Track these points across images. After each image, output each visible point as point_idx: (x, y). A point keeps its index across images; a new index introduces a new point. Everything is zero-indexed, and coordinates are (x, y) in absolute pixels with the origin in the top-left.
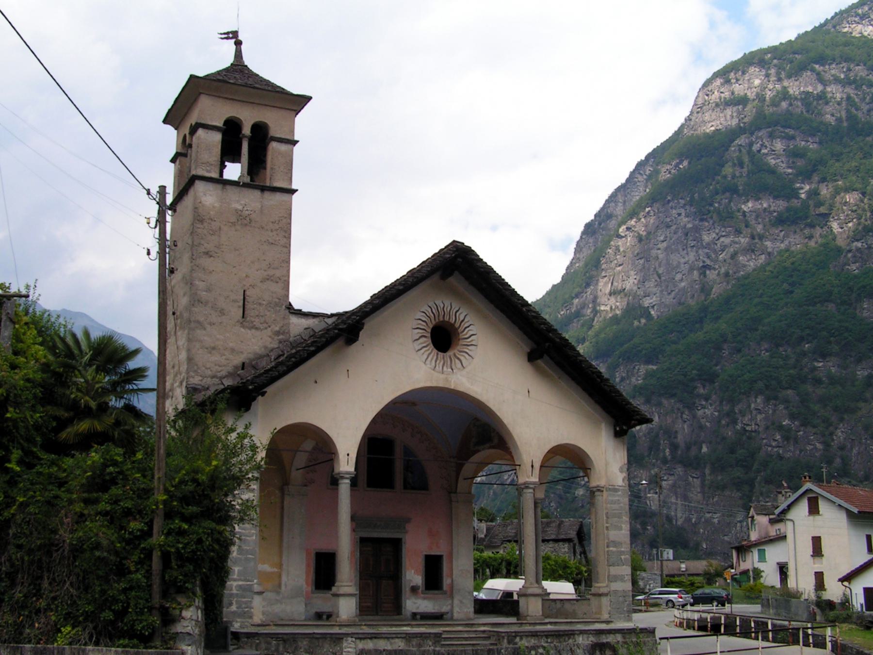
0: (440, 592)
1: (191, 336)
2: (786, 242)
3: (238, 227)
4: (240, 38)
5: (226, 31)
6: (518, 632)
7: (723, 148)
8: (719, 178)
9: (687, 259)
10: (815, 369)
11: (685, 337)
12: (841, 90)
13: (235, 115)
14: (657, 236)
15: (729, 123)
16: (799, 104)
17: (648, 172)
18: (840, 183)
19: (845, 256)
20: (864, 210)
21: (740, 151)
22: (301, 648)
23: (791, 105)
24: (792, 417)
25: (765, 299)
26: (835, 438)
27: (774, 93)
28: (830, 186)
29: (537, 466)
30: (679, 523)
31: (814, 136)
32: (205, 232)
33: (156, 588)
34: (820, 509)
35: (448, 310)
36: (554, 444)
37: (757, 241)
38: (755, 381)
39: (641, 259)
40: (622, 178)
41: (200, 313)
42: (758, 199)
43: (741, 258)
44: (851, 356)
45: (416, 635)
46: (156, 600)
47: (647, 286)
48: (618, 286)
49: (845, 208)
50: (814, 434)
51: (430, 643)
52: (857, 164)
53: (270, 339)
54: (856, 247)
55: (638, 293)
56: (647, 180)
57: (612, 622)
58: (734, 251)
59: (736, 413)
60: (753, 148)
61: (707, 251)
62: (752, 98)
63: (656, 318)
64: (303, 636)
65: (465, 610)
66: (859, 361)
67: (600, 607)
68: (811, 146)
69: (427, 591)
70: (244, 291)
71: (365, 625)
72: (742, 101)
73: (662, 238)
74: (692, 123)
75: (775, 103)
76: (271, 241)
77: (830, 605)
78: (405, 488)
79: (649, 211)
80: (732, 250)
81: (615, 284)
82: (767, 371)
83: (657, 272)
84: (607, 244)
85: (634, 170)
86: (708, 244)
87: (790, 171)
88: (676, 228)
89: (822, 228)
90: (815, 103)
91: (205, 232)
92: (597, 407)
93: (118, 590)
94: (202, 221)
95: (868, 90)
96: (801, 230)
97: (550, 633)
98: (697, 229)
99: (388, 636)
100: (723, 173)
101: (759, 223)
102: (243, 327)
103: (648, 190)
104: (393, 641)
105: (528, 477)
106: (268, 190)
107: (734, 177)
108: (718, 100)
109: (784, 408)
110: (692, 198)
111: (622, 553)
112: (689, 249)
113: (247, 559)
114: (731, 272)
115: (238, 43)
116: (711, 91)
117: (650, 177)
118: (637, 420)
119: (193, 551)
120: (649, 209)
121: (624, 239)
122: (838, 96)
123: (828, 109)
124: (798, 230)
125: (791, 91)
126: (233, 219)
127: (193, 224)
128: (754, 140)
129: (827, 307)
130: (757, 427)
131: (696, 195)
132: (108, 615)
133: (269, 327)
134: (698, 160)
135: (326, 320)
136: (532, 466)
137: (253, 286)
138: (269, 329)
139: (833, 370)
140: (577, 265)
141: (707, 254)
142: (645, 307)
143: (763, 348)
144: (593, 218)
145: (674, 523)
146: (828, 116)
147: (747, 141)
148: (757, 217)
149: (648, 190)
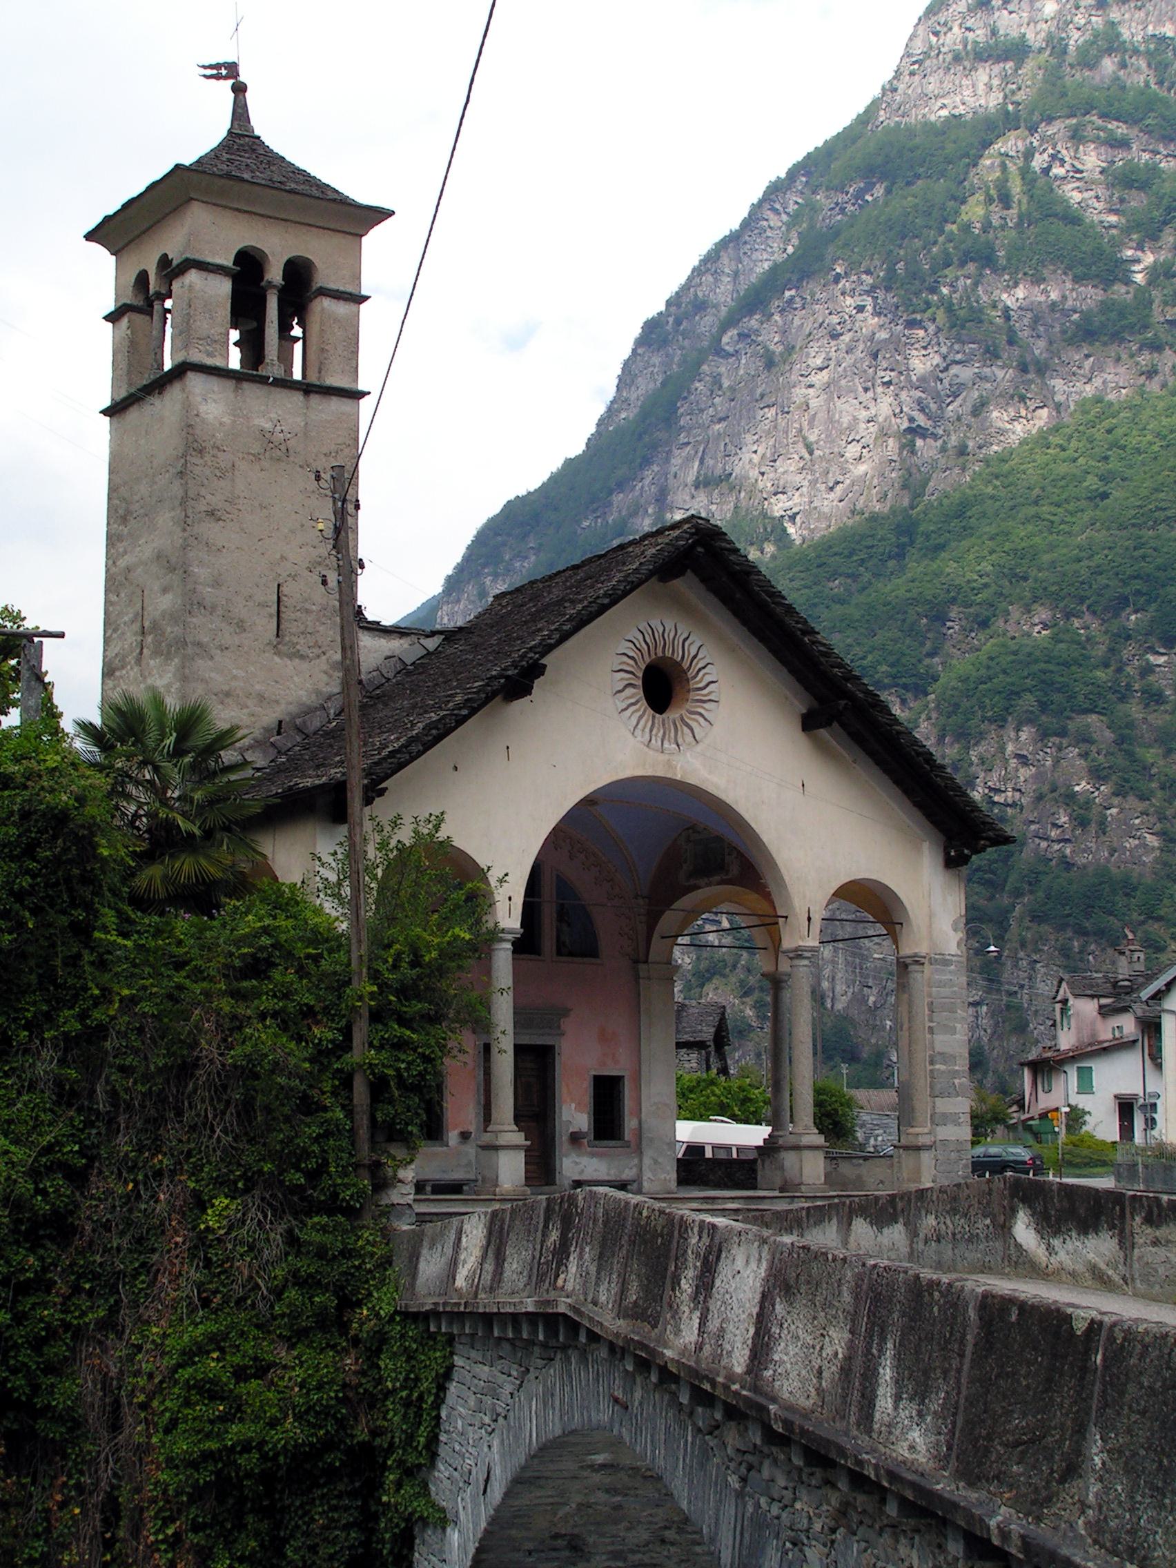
0: (619, 1143)
1: (187, 671)
2: (1097, 382)
3: (265, 464)
4: (243, 78)
5: (213, 62)
8: (954, 227)
9: (874, 412)
10: (1148, 670)
11: (864, 589)
13: (253, 244)
14: (808, 355)
15: (982, 102)
16: (1143, 64)
17: (792, 208)
21: (1004, 167)
23: (1123, 65)
24: (1097, 775)
27: (1087, 36)
29: (817, 919)
30: (839, 1006)
32: (208, 472)
33: (364, 1133)
36: (844, 879)
39: (768, 406)
40: (732, 221)
42: (1038, 280)
43: (995, 414)
46: (364, 1152)
47: (781, 470)
48: (714, 467)
50: (1142, 813)
53: (325, 678)
55: (761, 485)
56: (789, 227)
58: (981, 396)
59: (971, 764)
60: (1034, 164)
61: (918, 394)
62: (1037, 45)
65: (662, 1177)
67: (918, 1171)
72: (1016, 51)
73: (819, 362)
75: (1088, 60)
79: (793, 297)
81: (710, 462)
83: (805, 439)
84: (692, 370)
86: (922, 379)
87: (1113, 219)
88: (852, 340)
91: (208, 472)
92: (918, 814)
93: (310, 1137)
96: (1132, 356)
100: (965, 218)
101: (1039, 337)
102: (278, 653)
105: (802, 938)
106: (317, 392)
107: (987, 226)
109: (1080, 755)
110: (891, 271)
111: (955, 1074)
112: (880, 389)
114: (971, 444)
115: (239, 90)
116: (945, 24)
117: (795, 218)
119: (420, 1074)
120: (793, 292)
124: (1124, 356)
125: (1126, 34)
126: (256, 448)
127: (184, 456)
128: (1036, 144)
130: (1017, 794)
133: (324, 653)
135: (422, 641)
136: (809, 919)
137: (294, 577)
142: (774, 518)
145: (829, 1006)
147: (1020, 143)
148: (1036, 320)
149: (790, 250)
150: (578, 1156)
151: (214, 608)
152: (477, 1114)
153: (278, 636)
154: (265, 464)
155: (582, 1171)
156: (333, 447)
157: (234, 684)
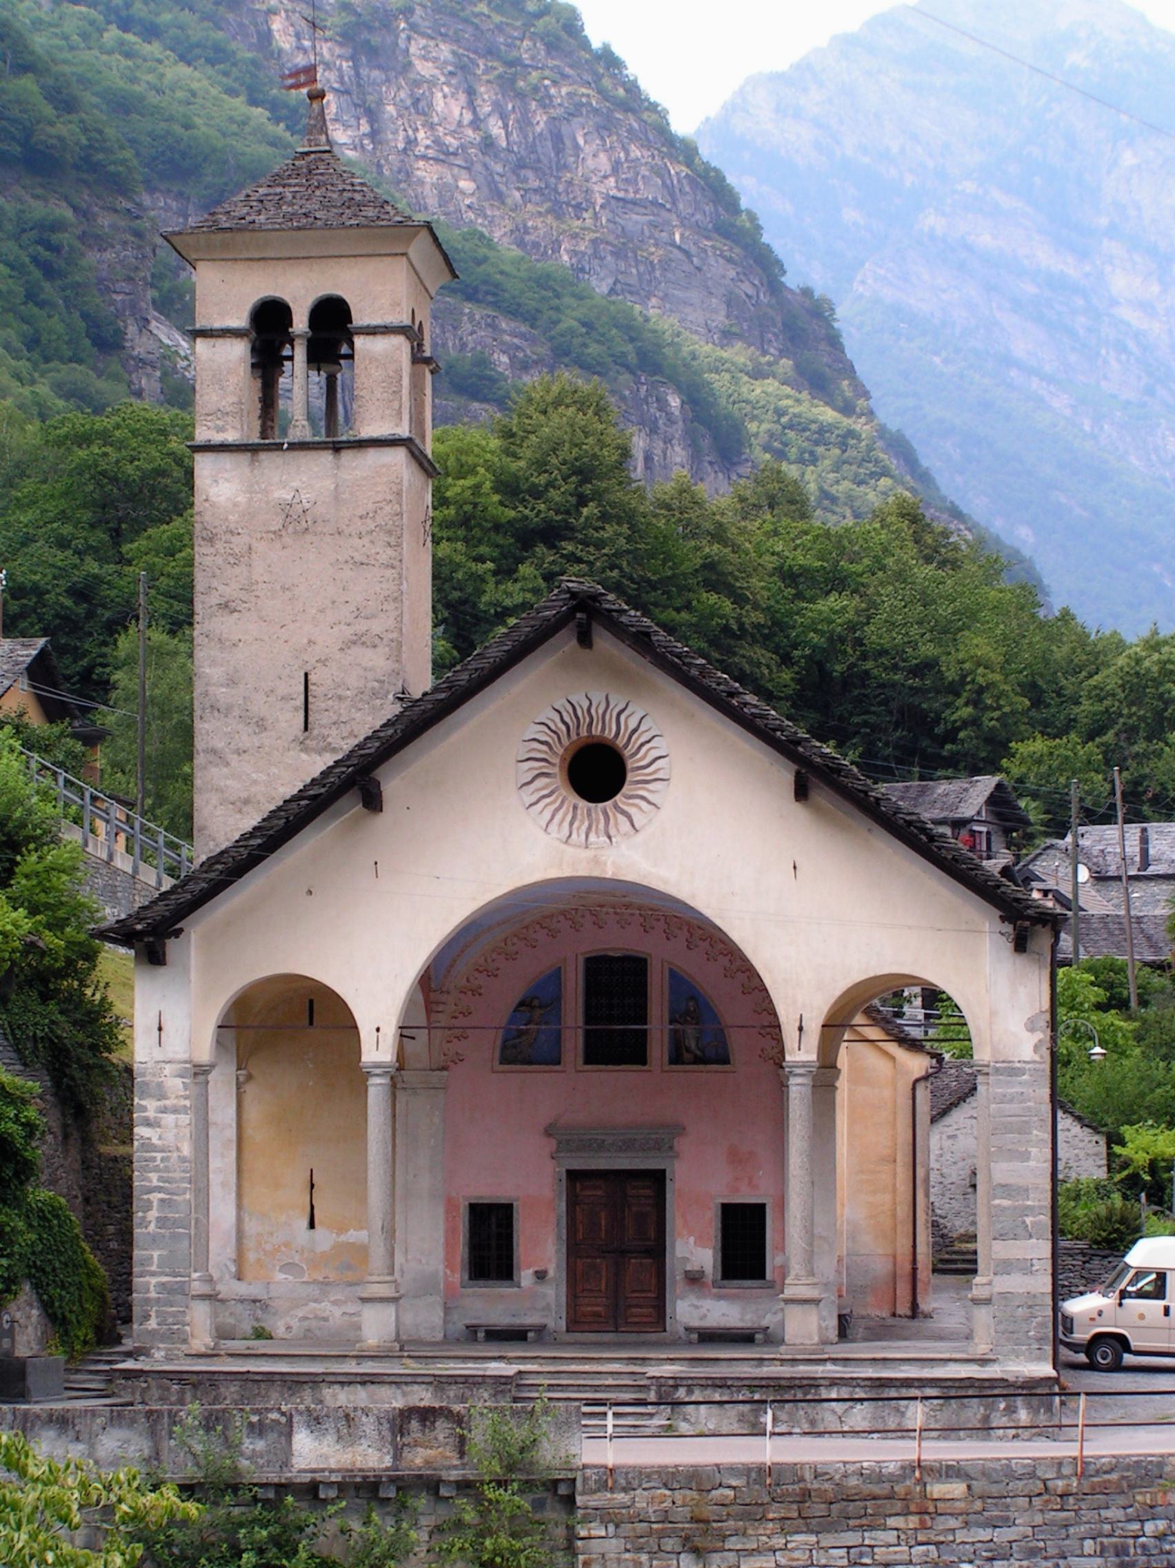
6: (681, 1378)
22: (225, 1399)
35: (601, 711)
45: (454, 1380)
51: (486, 1395)
57: (994, 1361)
64: (232, 1377)
69: (726, 1282)
70: (306, 675)
71: (409, 1357)
76: (358, 558)
91: (219, 560)
97: (756, 1383)
99: (398, 1379)
102: (306, 750)
104: (407, 1389)
113: (175, 1237)
136: (801, 1029)
137: (324, 662)
150: (698, 1298)
151: (229, 709)
152: (557, 1251)
153: (306, 729)
154: (287, 540)
155: (705, 1316)
156: (371, 507)
157: (253, 790)
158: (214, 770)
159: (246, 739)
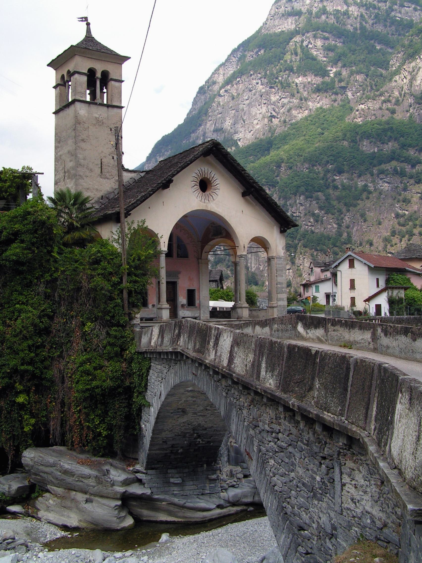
2: (321, 103)
3: (97, 126)
7: (286, 43)
8: (282, 61)
9: (261, 111)
10: (334, 180)
11: (259, 159)
12: (357, 10)
15: (290, 27)
16: (333, 17)
17: (239, 56)
18: (354, 68)
19: (355, 113)
20: (367, 86)
21: (296, 45)
23: (327, 18)
24: (321, 208)
25: (307, 137)
26: (344, 221)
27: (318, 10)
28: (348, 70)
31: (340, 38)
32: (82, 129)
33: (126, 305)
34: (355, 265)
37: (303, 101)
38: (300, 187)
41: (81, 171)
42: (305, 76)
43: (294, 112)
44: (355, 173)
49: (356, 84)
52: (364, 57)
53: (114, 184)
54: (361, 108)
55: (231, 131)
56: (238, 61)
59: (287, 206)
60: (304, 44)
61: (273, 106)
62: (304, 12)
63: (241, 146)
66: (359, 176)
68: (338, 45)
73: (246, 98)
74: (267, 26)
75: (318, 16)
77: (360, 313)
78: (178, 257)
80: (288, 106)
81: (217, 125)
82: (307, 181)
83: (243, 119)
85: (230, 55)
86: (274, 102)
87: (325, 59)
89: (342, 95)
90: (342, 17)
91: (82, 129)
92: (273, 219)
94: (80, 124)
95: (373, 11)
96: (330, 96)
98: (267, 93)
100: (285, 59)
102: (101, 178)
103: (238, 67)
107: (291, 61)
108: (284, 12)
109: (316, 203)
110: (266, 74)
112: (263, 105)
114: (287, 120)
115: (88, 24)
118: (291, 225)
119: (141, 289)
120: (239, 79)
121: (223, 97)
122: (356, 14)
123: (349, 21)
124: (328, 96)
125: (328, 9)
126: (94, 122)
127: (75, 125)
129: (343, 143)
130: (300, 214)
131: (268, 71)
132: (108, 318)
134: (270, 49)
137: (105, 157)
138: (114, 179)
139: (345, 181)
140: (194, 112)
141: (273, 109)
142: (234, 140)
143: (305, 167)
144: (204, 83)
146: (349, 26)
148: (304, 86)
149: (238, 67)
151: (84, 165)
158: (80, 180)
159: (88, 173)
